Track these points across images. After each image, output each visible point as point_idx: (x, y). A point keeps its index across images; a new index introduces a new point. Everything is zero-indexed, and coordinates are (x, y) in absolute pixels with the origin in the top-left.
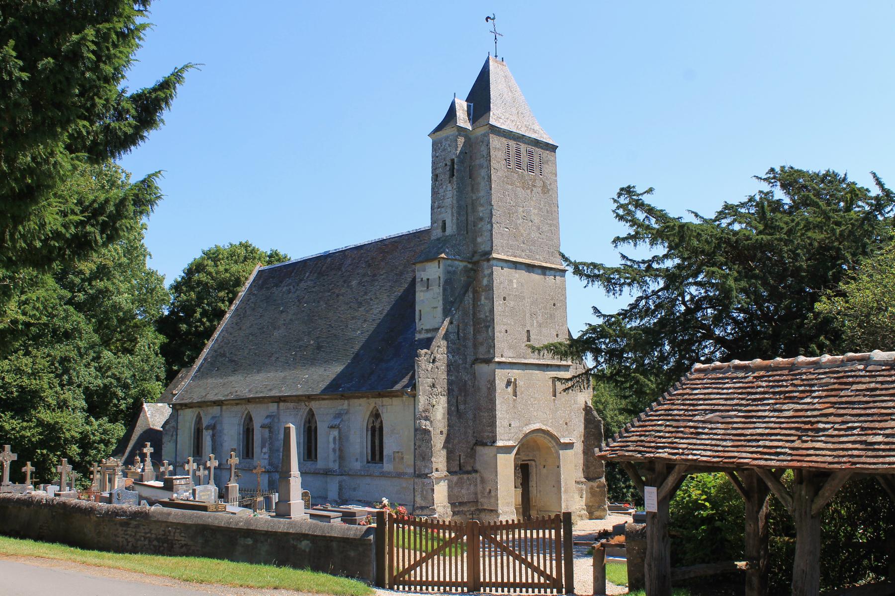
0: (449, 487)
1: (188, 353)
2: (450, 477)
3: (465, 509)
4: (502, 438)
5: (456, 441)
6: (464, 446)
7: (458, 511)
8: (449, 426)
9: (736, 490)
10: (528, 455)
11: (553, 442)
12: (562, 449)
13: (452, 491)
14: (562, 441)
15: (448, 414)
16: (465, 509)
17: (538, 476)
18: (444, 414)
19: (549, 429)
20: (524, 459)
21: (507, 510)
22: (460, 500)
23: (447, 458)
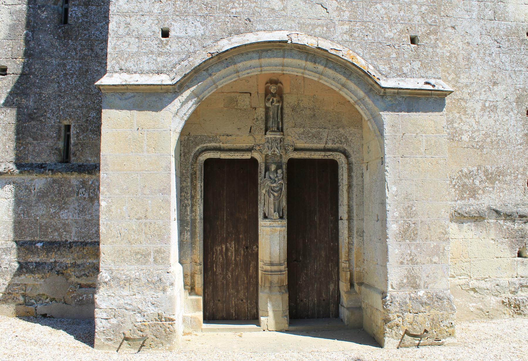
0: (18, 201)
1: (41, 36)
2: (18, 177)
3: (68, 260)
4: (124, 64)
5: (50, 91)
6: (75, 103)
7: (38, 264)
8: (27, 54)
9: (191, 155)
10: (317, 136)
11: (351, 85)
12: (392, 108)
13: (26, 213)
14: (384, 83)
15: (28, 25)
16: (68, 260)
17: (355, 190)
18: (13, 28)
19: (326, 45)
20: (300, 144)
21: (134, 274)
22: (55, 236)
23: (18, 132)
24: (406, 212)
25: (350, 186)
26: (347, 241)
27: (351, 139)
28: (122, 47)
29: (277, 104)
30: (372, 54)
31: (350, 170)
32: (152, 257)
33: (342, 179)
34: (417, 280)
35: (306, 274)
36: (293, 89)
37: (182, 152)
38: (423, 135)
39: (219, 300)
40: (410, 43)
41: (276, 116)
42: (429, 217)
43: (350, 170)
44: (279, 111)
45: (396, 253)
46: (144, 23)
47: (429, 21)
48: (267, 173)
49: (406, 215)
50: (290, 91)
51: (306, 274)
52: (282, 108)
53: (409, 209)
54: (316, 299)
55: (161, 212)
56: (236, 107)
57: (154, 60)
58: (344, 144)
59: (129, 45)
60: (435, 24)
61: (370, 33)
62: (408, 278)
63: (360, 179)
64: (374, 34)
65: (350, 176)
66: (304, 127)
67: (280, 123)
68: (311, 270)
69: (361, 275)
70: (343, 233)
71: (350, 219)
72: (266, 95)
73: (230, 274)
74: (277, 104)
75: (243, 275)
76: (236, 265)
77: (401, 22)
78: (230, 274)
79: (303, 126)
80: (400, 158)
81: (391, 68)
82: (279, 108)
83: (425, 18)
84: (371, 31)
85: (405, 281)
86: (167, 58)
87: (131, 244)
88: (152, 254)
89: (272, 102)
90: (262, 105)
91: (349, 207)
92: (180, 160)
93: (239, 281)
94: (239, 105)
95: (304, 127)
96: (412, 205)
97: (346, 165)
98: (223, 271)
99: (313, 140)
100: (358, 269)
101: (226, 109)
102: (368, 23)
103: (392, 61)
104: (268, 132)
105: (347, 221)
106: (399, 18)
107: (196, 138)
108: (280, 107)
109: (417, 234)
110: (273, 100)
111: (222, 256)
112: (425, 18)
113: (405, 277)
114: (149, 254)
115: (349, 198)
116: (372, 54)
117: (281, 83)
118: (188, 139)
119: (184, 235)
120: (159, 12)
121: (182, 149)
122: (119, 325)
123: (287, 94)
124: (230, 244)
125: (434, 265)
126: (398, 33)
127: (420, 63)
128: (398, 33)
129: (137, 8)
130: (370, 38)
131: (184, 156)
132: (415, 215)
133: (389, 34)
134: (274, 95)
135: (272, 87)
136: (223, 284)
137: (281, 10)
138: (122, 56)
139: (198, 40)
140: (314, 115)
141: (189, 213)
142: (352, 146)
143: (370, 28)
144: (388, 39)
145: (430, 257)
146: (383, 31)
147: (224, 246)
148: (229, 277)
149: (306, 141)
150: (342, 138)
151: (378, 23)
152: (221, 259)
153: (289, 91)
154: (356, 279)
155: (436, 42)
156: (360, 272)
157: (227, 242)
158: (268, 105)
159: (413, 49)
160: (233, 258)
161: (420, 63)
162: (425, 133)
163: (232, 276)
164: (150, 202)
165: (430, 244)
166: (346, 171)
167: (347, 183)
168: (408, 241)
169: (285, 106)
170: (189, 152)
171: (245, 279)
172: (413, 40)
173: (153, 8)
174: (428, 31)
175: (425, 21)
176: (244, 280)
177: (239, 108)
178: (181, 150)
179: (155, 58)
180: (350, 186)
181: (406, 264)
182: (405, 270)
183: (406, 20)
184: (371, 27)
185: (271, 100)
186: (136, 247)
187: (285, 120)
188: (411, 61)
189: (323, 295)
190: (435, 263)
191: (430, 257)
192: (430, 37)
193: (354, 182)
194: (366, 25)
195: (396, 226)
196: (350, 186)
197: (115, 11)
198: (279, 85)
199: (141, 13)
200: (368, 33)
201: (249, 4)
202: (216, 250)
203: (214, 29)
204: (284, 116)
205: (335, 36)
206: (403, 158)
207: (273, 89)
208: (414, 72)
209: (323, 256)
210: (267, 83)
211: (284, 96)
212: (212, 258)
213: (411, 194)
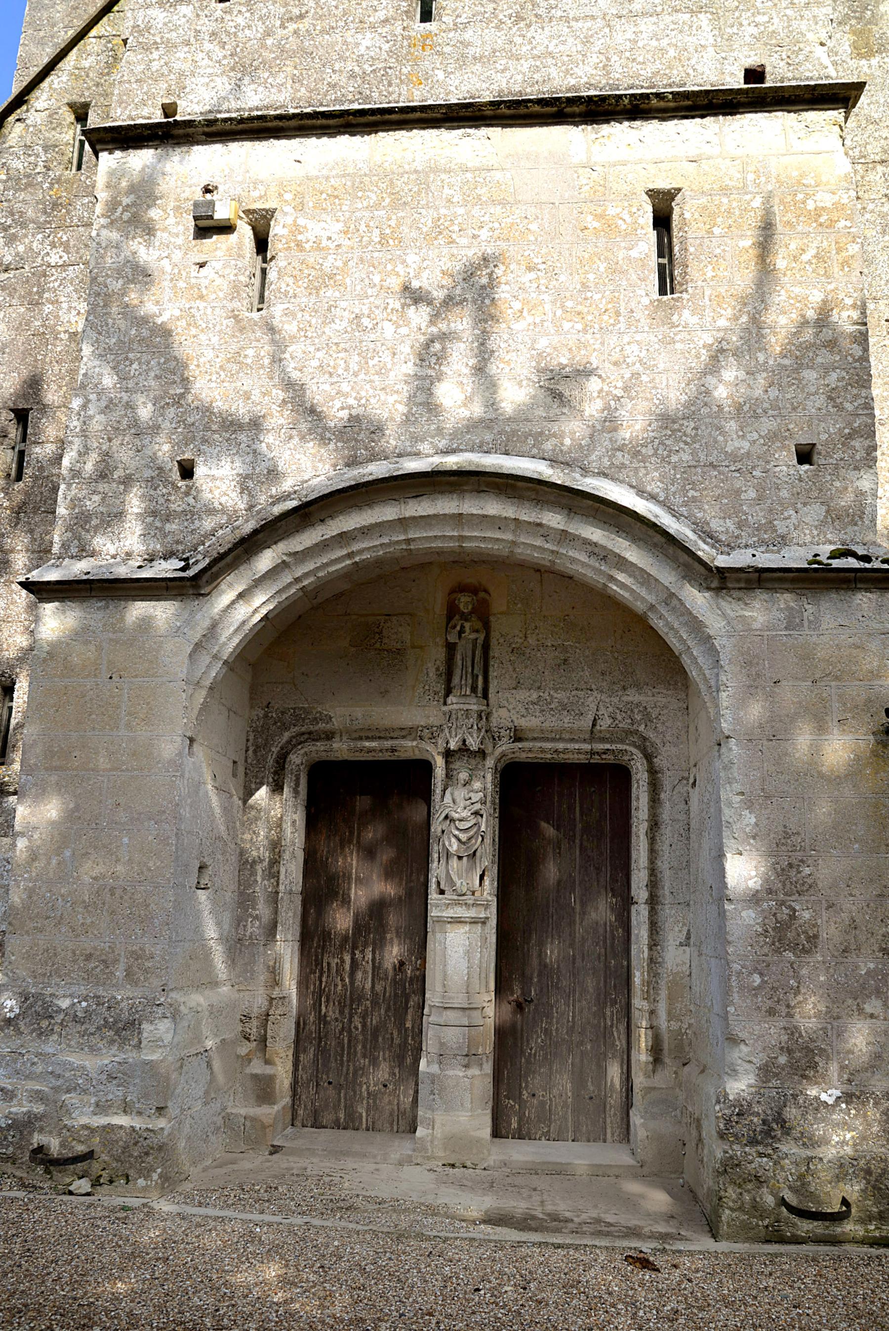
24: (782, 878)
25: (654, 825)
26: (646, 955)
27: (657, 713)
28: (88, 503)
29: (473, 636)
30: (691, 493)
31: (655, 787)
32: (122, 966)
33: (637, 809)
34: (817, 1059)
35: (547, 1032)
36: (516, 604)
37: (250, 744)
38: (833, 684)
39: (330, 1083)
40: (795, 461)
41: (469, 664)
42: (851, 895)
43: (655, 787)
44: (478, 653)
45: (756, 984)
46: (139, 451)
47: (848, 406)
48: (448, 792)
49: (784, 885)
50: (508, 607)
51: (547, 1032)
52: (486, 647)
53: (793, 873)
54: (570, 1094)
55: (151, 864)
56: (378, 645)
57: (157, 528)
58: (640, 725)
59: (103, 499)
60: (866, 412)
61: (686, 443)
62: (790, 1051)
63: (682, 806)
64: (697, 446)
65: (655, 801)
66: (539, 688)
67: (480, 679)
68: (557, 1023)
69: (682, 1040)
70: (637, 935)
71: (653, 901)
72: (450, 618)
73: (357, 1022)
74: (473, 636)
75: (390, 1026)
76: (375, 1003)
77: (770, 412)
78: (357, 1022)
79: (538, 684)
80: (765, 743)
81: (740, 525)
82: (479, 647)
83: (838, 401)
84: (689, 440)
85: (783, 1060)
86: (186, 524)
87: (77, 936)
88: (123, 959)
89: (461, 632)
90: (440, 641)
91: (653, 872)
92: (246, 761)
93: (380, 1039)
94: (386, 641)
95: (539, 688)
96: (802, 861)
97: (646, 775)
98: (342, 1012)
99: (561, 717)
100: (674, 1025)
101: (353, 649)
102: (681, 422)
103: (745, 508)
104: (450, 699)
105: (646, 906)
106: (766, 405)
107: (283, 713)
108: (480, 642)
109: (816, 936)
110: (462, 627)
111: (342, 980)
112: (838, 401)
113: (782, 1049)
114: (116, 961)
115: (653, 852)
116: (691, 493)
117: (486, 591)
118: (266, 716)
119: (245, 926)
120: (174, 425)
121: (251, 738)
122: (30, 1122)
123: (501, 613)
124: (362, 952)
125: (869, 1021)
126: (762, 441)
127: (824, 508)
128: (762, 441)
129: (125, 422)
130: (686, 457)
131: (255, 752)
132: (810, 887)
133: (737, 444)
134: (465, 617)
135: (463, 599)
136: (340, 1044)
137: (460, 407)
138: (86, 522)
139: (259, 482)
140: (565, 660)
141: (259, 879)
142: (661, 728)
143: (685, 435)
144: (734, 457)
145: (855, 999)
146: (720, 438)
147: (347, 958)
148: (357, 1029)
149: (543, 719)
150: (636, 711)
151: (707, 420)
152: (340, 987)
153: (504, 608)
154: (670, 1050)
155: (868, 454)
156: (679, 1032)
157: (354, 947)
158: (453, 638)
159: (804, 476)
160: (368, 985)
161: (824, 508)
162: (837, 678)
163: (364, 1025)
164: (126, 840)
165: (857, 967)
166: (645, 788)
167: (646, 817)
168: (791, 954)
169: (493, 642)
170: (266, 745)
171: (395, 1034)
172: (805, 455)
173: (160, 419)
174: (847, 431)
175: (840, 408)
176: (392, 1039)
177: (385, 647)
178: (248, 740)
179: (158, 524)
180: (654, 825)
181: (784, 1014)
182: (783, 1031)
183: (784, 407)
184: (689, 431)
185: (458, 628)
186: (88, 944)
187: (492, 674)
188: (799, 506)
189: (589, 1084)
190: (872, 1016)
191: (855, 999)
192: (853, 443)
193: (666, 813)
194: (676, 426)
195: (753, 915)
196: (656, 824)
197: (77, 430)
198: (482, 594)
199: (133, 431)
200: (682, 445)
201: (383, 398)
202: (329, 964)
203: (297, 456)
204: (492, 663)
205: (593, 457)
206: (774, 743)
207: (465, 602)
208: (807, 532)
209: (591, 990)
210: (452, 591)
211: (492, 618)
212: (318, 983)
213: (798, 833)
